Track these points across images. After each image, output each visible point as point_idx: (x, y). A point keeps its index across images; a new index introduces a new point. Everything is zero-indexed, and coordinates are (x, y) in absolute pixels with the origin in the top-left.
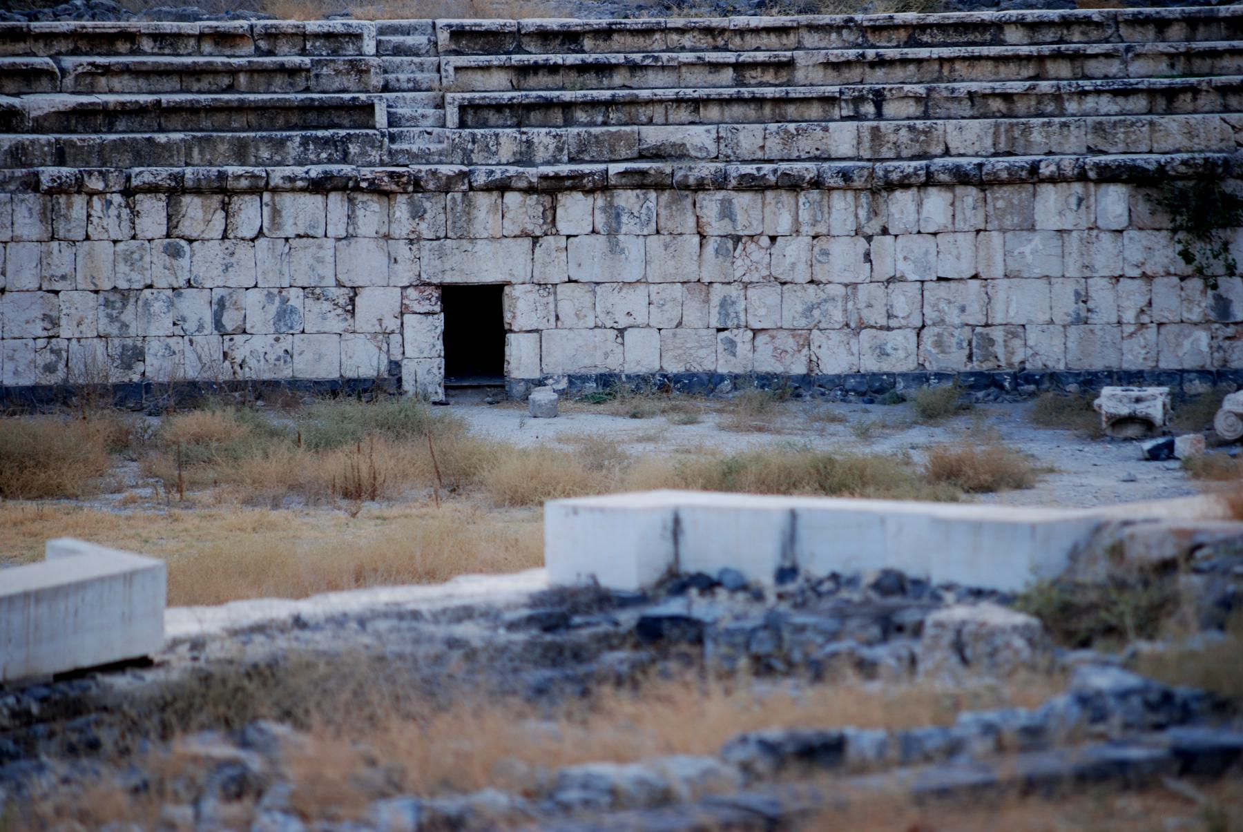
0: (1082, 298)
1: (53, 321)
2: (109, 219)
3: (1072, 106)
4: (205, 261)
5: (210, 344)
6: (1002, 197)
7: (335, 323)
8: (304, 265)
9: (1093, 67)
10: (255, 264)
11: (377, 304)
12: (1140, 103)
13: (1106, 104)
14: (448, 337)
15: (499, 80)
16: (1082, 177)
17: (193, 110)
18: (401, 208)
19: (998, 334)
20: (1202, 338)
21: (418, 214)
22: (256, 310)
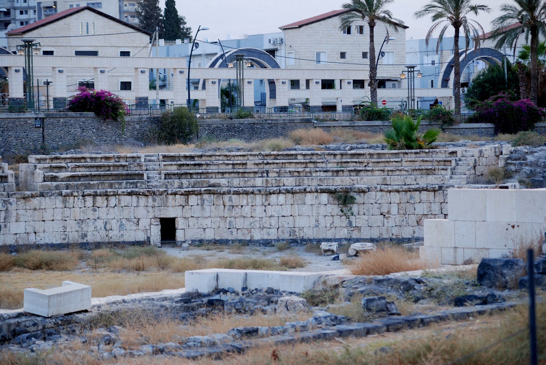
2: (79, 202)
3: (314, 174)
4: (102, 212)
5: (103, 233)
6: (297, 196)
7: (134, 227)
8: (126, 213)
9: (319, 165)
10: (115, 213)
11: (144, 223)
12: (330, 174)
13: (322, 174)
14: (162, 231)
15: (175, 168)
16: (317, 191)
19: (297, 230)
20: (345, 230)
21: (154, 200)
22: (114, 224)
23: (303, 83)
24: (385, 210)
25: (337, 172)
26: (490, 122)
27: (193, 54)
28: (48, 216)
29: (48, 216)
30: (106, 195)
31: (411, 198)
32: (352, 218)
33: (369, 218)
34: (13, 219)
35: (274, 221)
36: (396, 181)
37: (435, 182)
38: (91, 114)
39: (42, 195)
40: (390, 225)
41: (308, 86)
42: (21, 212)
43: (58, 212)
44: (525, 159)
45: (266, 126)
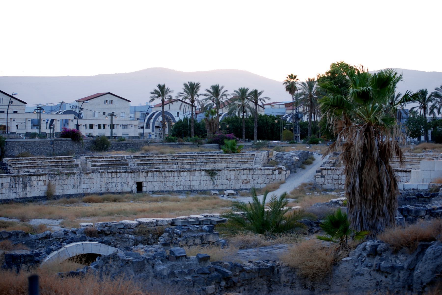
0: (200, 182)
1: (101, 186)
5: (115, 188)
6: (192, 173)
8: (124, 180)
10: (119, 180)
11: (131, 184)
12: (203, 163)
13: (200, 163)
14: (137, 187)
15: (139, 161)
16: (200, 171)
17: (112, 164)
18: (133, 174)
20: (212, 186)
21: (134, 175)
22: (119, 185)
23: (102, 126)
24: (228, 178)
25: (207, 162)
26: (216, 143)
27: (162, 107)
28: (95, 181)
29: (95, 181)
30: (116, 173)
31: (240, 173)
32: (215, 181)
33: (221, 181)
34: (83, 182)
35: (182, 183)
36: (232, 166)
37: (249, 166)
38: (70, 139)
39: (93, 172)
40: (231, 183)
41: (104, 128)
42: (85, 179)
43: (99, 179)
44: (283, 157)
45: (131, 145)
